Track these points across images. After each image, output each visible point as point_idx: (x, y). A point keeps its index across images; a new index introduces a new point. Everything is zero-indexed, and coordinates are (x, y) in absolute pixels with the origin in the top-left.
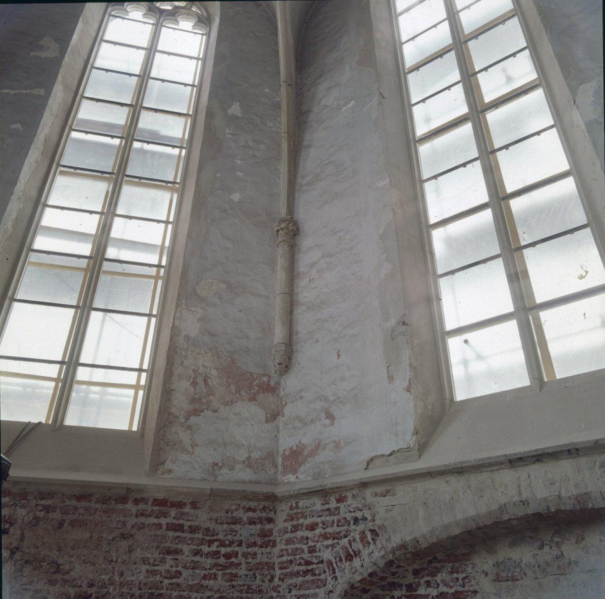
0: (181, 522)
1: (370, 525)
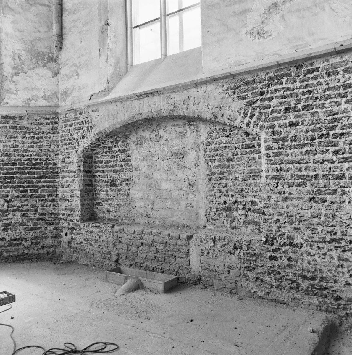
0: (15, 125)
1: (90, 124)
